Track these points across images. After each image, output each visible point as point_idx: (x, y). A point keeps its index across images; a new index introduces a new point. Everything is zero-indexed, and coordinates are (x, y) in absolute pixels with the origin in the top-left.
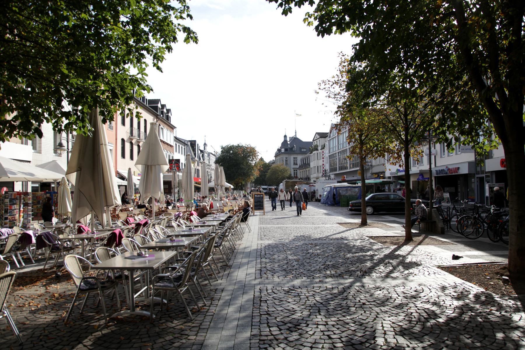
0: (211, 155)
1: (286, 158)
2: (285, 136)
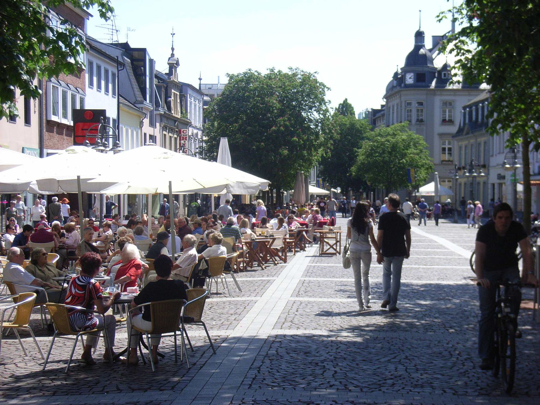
0: (190, 92)
1: (421, 104)
2: (419, 35)
